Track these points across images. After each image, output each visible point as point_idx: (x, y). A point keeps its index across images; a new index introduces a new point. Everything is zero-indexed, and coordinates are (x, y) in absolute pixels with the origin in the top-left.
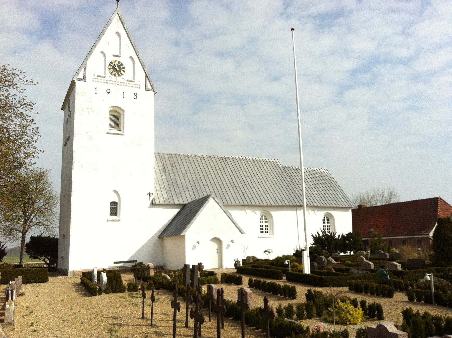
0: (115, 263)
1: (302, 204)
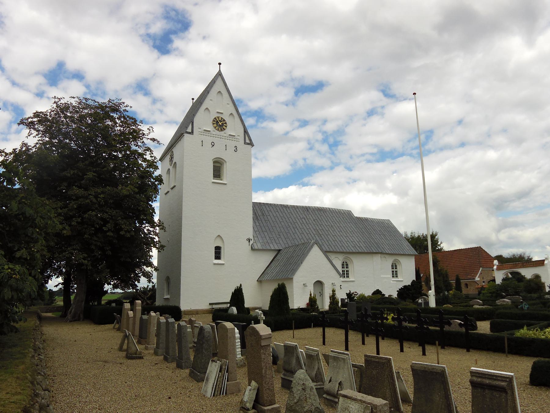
0: (210, 304)
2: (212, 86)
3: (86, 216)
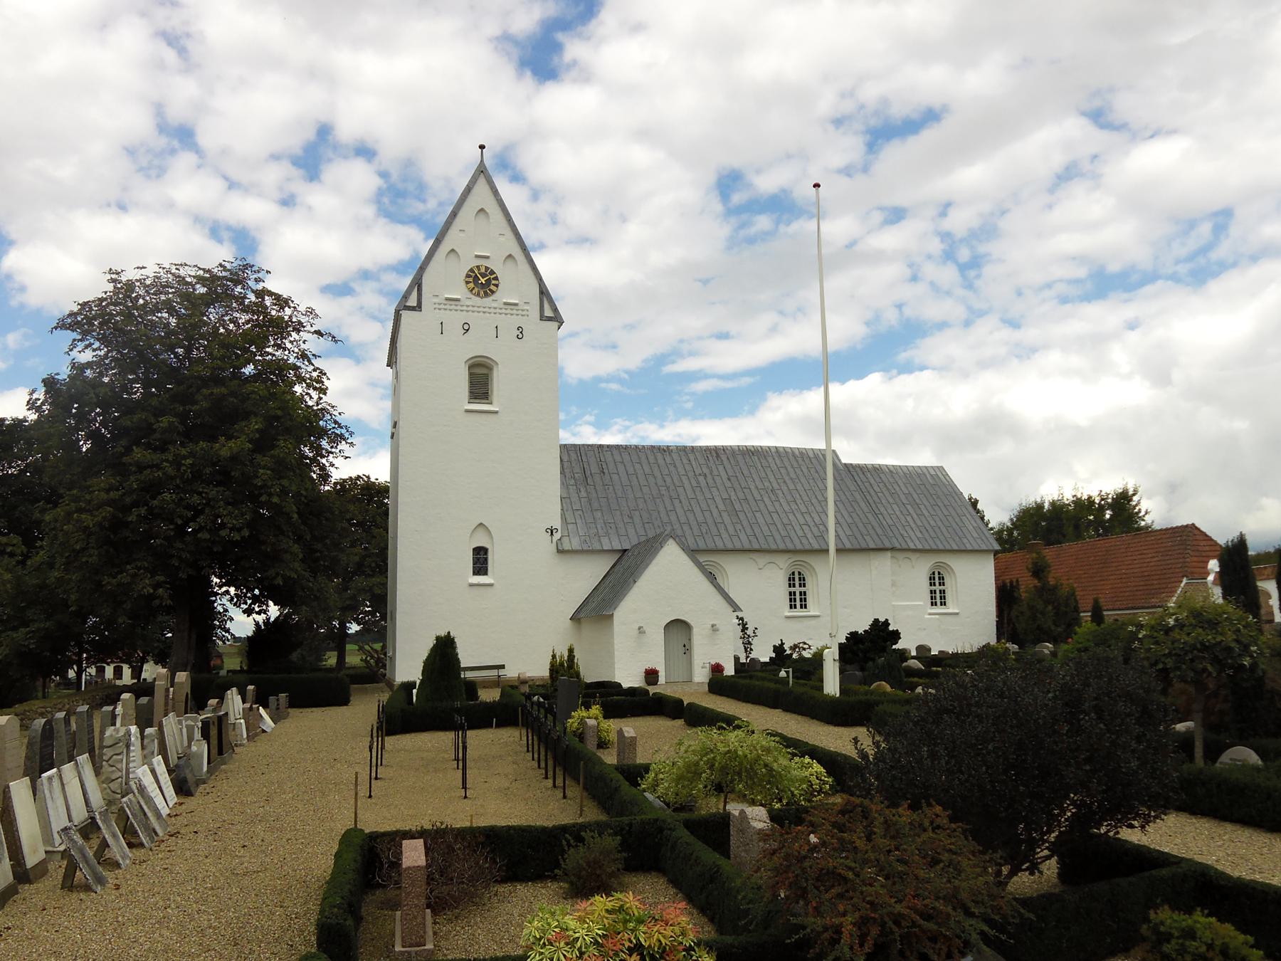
1: (824, 547)
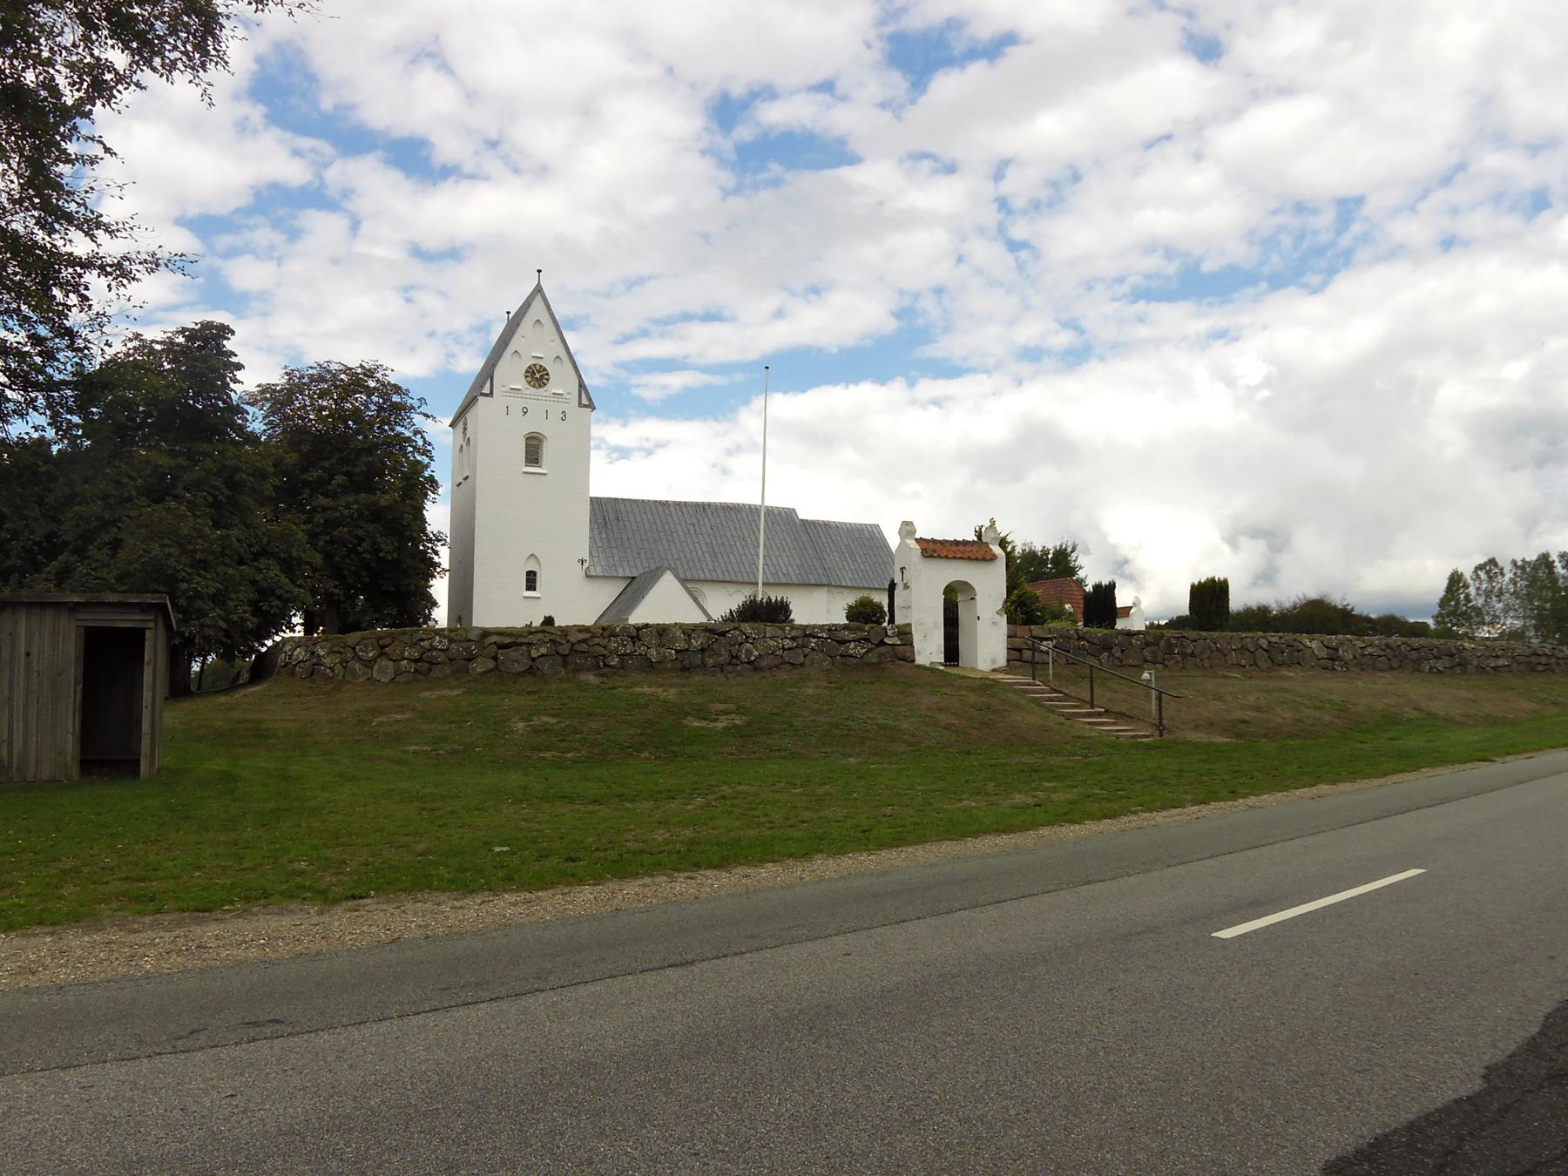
2: (525, 313)
3: (335, 533)
